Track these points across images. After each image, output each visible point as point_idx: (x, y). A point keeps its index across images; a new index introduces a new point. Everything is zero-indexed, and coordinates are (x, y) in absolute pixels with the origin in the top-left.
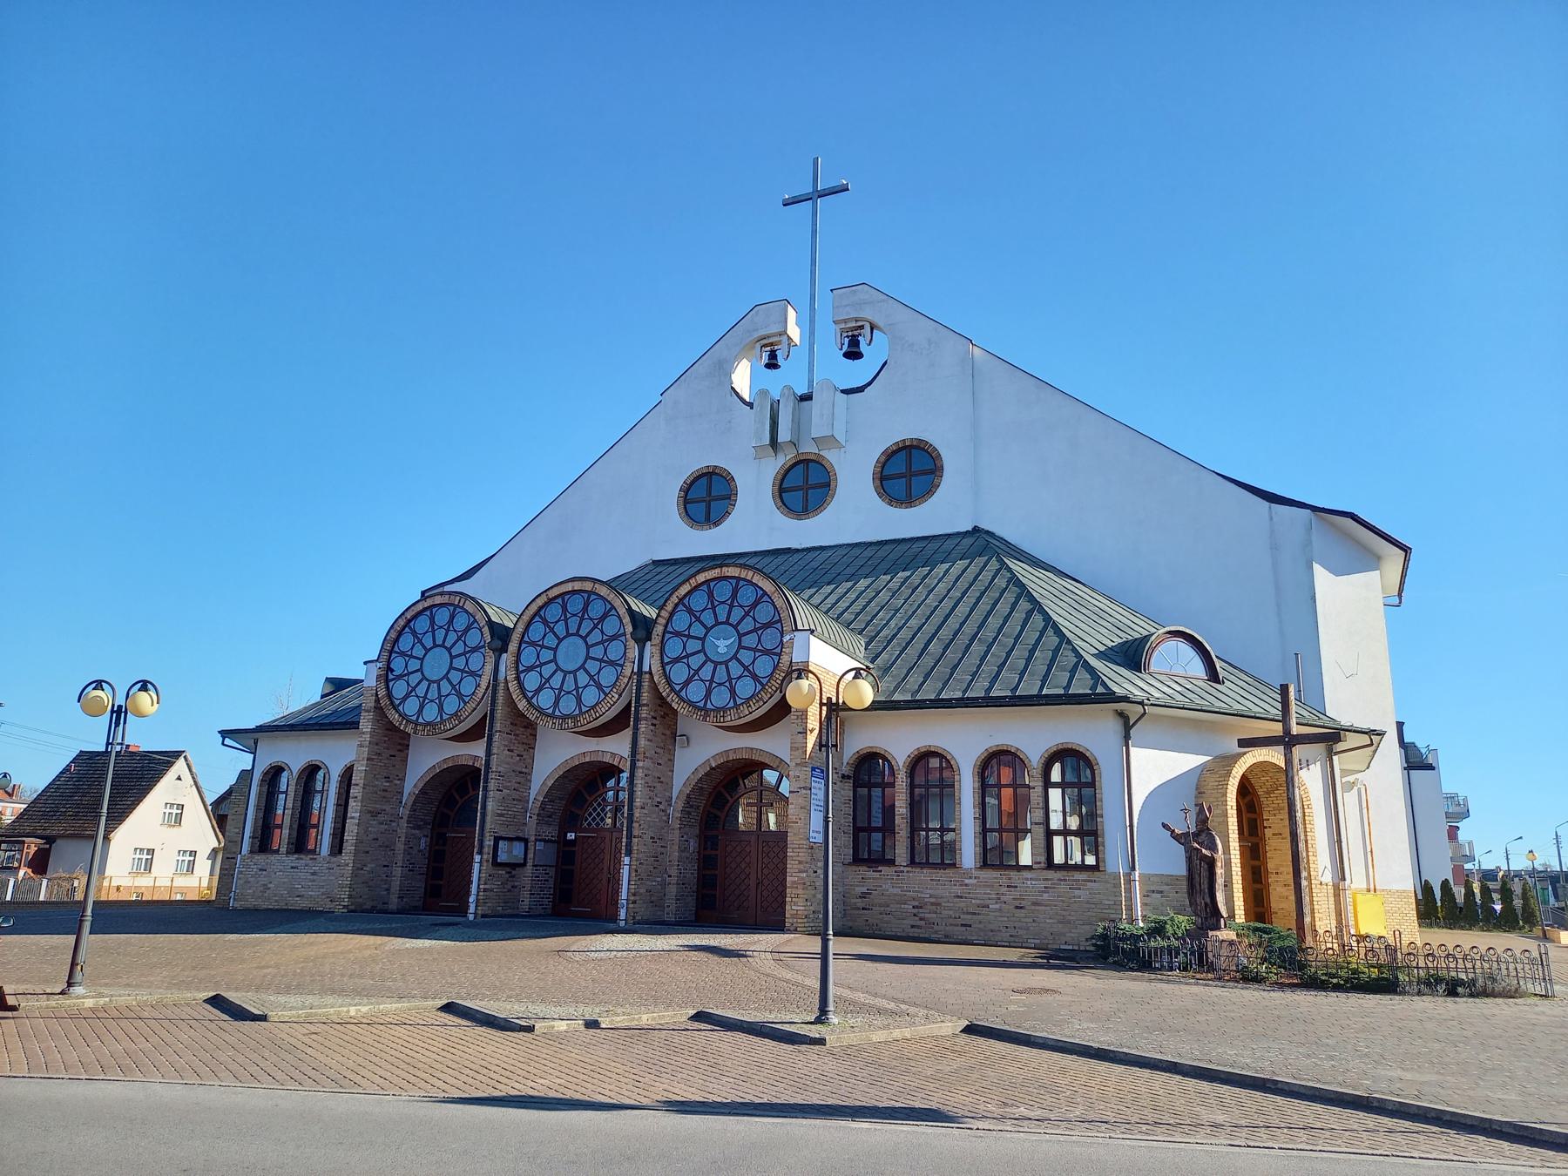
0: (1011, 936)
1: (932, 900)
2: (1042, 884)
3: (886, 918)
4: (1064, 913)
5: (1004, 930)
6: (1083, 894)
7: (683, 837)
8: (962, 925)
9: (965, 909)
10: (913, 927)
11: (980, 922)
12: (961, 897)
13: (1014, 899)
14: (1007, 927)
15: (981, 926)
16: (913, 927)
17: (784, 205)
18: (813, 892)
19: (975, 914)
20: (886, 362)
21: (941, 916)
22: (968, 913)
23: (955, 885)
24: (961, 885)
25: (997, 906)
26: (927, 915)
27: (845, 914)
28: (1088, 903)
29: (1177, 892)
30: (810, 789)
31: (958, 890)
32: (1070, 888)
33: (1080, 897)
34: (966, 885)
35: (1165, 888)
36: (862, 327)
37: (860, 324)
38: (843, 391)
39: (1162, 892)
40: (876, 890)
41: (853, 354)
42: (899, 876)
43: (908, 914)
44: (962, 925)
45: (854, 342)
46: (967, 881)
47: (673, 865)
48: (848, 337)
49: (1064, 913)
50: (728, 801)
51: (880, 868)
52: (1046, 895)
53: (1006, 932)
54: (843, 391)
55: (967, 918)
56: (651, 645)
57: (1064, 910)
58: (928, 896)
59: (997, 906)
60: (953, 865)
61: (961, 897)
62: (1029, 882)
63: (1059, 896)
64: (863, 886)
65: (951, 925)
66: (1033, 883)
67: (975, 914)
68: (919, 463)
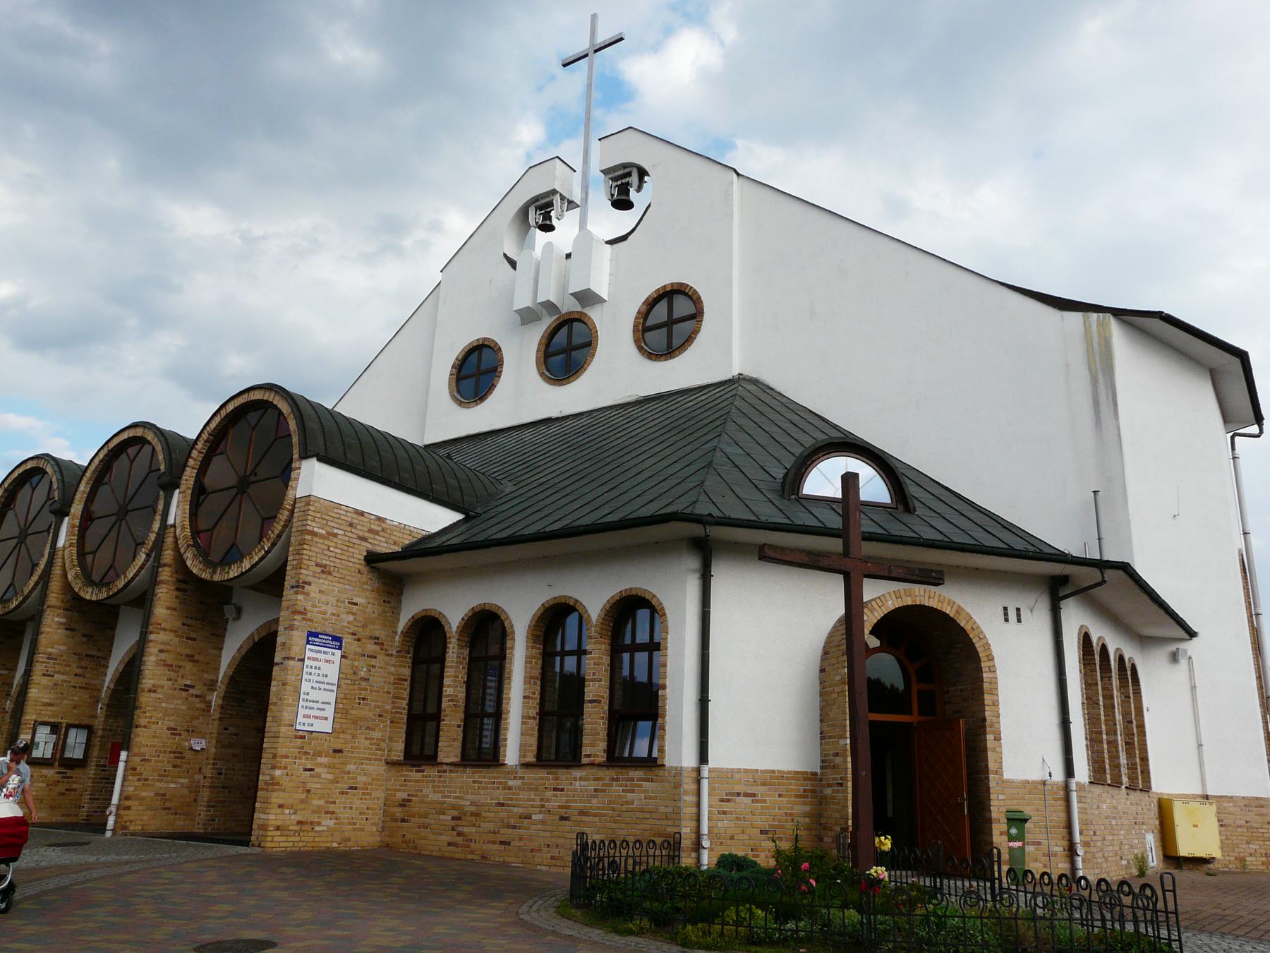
0: (552, 858)
1: (473, 809)
2: (592, 785)
3: (423, 832)
4: (613, 825)
5: (545, 849)
6: (637, 798)
7: (226, 729)
8: (501, 843)
9: (505, 821)
10: (449, 844)
11: (521, 839)
12: (503, 805)
13: (560, 807)
14: (548, 845)
15: (521, 843)
16: (449, 844)
17: (565, 65)
18: (304, 796)
19: (514, 827)
20: (649, 205)
21: (481, 830)
22: (509, 827)
23: (498, 788)
24: (504, 788)
25: (540, 817)
26: (466, 830)
27: (383, 827)
28: (642, 811)
29: (780, 796)
30: (303, 660)
31: (500, 795)
32: (623, 791)
33: (633, 803)
34: (510, 788)
35: (760, 790)
36: (629, 174)
37: (627, 170)
38: (607, 242)
39: (754, 795)
40: (416, 796)
41: (622, 203)
42: (440, 777)
43: (447, 828)
44: (501, 843)
45: (624, 189)
46: (511, 783)
47: (209, 764)
48: (617, 186)
49: (613, 825)
50: (871, 710)
51: (422, 768)
52: (594, 801)
53: (548, 852)
54: (607, 242)
55: (507, 833)
56: (180, 493)
57: (615, 822)
58: (469, 803)
59: (540, 817)
60: (651, 763)
61: (503, 805)
62: (577, 783)
63: (610, 802)
64: (404, 791)
65: (489, 842)
66: (583, 783)
67: (514, 827)
68: (682, 307)
